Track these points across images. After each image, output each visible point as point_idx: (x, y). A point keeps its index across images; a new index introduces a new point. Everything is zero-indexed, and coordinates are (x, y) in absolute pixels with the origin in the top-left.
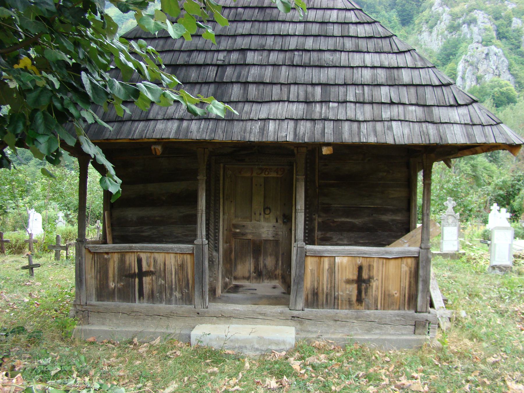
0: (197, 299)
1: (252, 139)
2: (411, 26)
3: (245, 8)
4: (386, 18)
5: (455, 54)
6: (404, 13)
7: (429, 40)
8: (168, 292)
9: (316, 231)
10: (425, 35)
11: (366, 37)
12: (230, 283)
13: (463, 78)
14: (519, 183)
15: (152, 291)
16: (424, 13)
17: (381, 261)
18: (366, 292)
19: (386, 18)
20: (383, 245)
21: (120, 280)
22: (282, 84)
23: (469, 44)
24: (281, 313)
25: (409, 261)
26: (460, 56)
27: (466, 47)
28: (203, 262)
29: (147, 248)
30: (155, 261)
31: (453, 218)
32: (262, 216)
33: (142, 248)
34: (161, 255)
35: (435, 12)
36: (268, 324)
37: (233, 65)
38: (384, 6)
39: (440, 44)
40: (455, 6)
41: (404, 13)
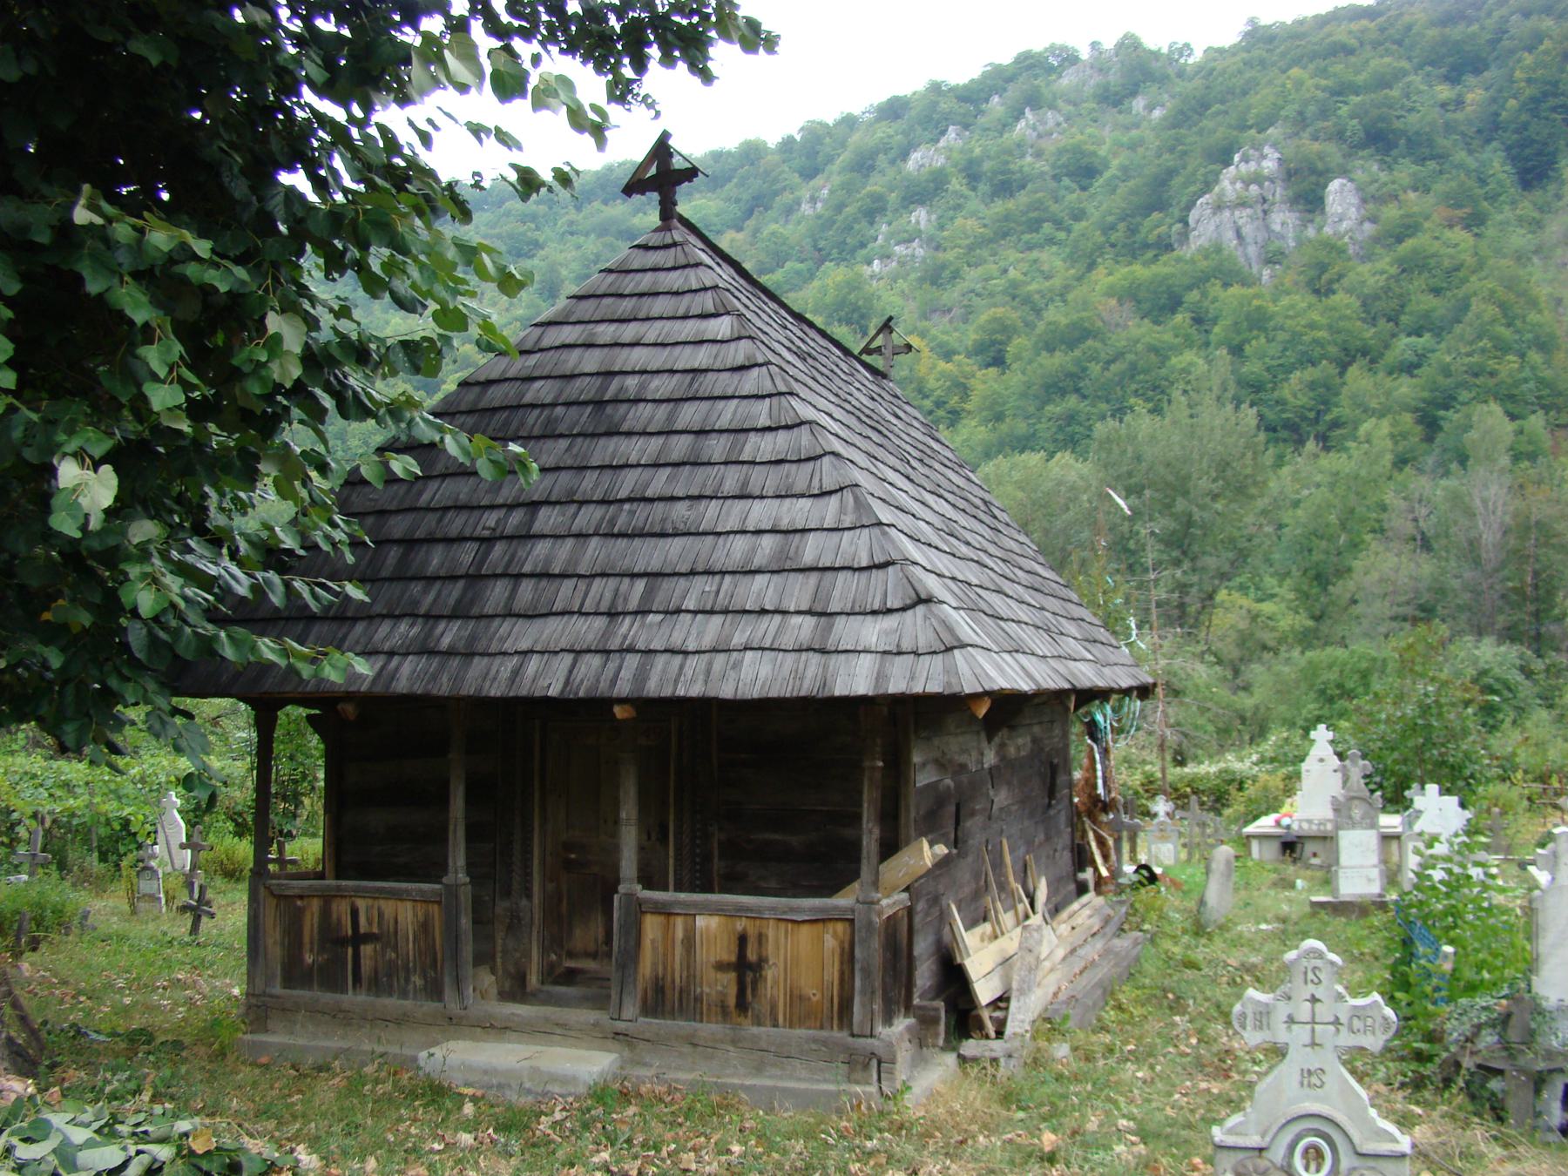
0: (449, 993)
1: (492, 693)
2: (1552, 188)
3: (568, 404)
4: (1468, 172)
6: (1528, 151)
9: (716, 860)
11: (770, 462)
17: (782, 925)
18: (754, 990)
19: (1468, 172)
22: (580, 576)
24: (596, 1025)
25: (840, 927)
29: (365, 889)
30: (381, 915)
31: (1364, 806)
33: (356, 889)
34: (391, 902)
36: (572, 1046)
38: (1463, 134)
41: (1528, 151)
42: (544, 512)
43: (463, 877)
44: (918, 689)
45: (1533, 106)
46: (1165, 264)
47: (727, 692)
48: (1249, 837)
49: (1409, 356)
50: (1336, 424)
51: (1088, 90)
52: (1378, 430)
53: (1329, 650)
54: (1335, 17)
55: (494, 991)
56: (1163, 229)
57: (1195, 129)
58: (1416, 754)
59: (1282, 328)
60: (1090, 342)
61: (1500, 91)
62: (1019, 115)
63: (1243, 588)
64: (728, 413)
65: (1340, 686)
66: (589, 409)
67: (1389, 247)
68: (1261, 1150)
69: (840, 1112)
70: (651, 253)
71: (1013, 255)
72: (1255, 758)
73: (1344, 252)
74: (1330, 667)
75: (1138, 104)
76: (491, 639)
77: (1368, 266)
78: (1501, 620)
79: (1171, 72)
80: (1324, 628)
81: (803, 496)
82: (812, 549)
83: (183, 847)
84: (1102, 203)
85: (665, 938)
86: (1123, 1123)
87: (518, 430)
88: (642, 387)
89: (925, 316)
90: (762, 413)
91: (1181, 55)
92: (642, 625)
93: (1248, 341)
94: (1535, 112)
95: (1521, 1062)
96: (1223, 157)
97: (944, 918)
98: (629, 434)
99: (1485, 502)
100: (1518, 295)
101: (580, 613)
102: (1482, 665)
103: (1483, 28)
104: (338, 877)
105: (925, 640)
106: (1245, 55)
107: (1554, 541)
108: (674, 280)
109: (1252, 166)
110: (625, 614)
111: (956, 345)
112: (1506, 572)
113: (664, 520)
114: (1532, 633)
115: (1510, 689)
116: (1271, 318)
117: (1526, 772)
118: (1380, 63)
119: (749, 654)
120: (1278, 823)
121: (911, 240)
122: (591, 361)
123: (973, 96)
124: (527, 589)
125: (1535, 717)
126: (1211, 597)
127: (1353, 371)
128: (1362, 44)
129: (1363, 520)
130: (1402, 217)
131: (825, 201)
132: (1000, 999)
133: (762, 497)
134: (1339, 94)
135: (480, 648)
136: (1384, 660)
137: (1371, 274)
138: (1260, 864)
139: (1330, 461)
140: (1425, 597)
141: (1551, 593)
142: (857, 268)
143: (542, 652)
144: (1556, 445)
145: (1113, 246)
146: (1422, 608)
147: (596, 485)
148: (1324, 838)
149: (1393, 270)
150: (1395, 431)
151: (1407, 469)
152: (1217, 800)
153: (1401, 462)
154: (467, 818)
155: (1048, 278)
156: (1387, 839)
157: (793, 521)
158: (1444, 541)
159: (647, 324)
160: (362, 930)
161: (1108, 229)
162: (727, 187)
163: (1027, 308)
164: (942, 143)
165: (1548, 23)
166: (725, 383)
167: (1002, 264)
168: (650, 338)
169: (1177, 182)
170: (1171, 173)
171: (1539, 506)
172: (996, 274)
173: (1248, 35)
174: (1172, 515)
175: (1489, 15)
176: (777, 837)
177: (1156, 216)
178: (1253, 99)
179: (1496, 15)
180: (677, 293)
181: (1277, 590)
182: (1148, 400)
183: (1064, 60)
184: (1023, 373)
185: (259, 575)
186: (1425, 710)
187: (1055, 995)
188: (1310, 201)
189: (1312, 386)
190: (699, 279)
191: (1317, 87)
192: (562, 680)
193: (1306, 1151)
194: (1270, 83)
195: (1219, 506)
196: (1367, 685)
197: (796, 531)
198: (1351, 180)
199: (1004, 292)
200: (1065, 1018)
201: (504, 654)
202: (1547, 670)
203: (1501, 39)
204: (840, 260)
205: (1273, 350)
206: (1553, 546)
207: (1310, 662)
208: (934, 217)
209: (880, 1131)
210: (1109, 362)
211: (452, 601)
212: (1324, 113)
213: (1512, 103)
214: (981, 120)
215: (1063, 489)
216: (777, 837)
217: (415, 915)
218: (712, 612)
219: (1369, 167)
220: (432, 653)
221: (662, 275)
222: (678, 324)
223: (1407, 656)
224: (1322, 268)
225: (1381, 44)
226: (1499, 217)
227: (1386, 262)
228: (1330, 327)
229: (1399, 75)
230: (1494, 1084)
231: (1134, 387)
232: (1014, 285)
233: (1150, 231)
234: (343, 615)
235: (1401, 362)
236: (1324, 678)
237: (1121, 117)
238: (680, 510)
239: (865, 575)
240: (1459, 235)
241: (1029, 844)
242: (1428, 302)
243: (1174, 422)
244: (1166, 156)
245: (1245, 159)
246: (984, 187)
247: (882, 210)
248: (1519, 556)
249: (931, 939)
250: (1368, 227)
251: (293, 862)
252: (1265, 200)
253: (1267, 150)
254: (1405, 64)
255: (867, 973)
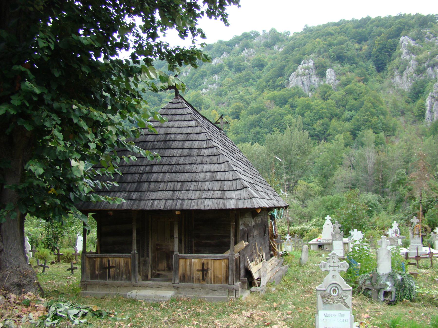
0: (133, 279)
2: (385, 72)
4: (363, 67)
5: (423, 92)
6: (379, 62)
7: (401, 82)
8: (121, 275)
10: (397, 78)
12: (156, 272)
13: (431, 111)
14: (432, 203)
15: (114, 275)
16: (394, 61)
17: (212, 261)
18: (206, 275)
20: (222, 253)
21: (100, 270)
22: (165, 182)
23: (434, 83)
24: (169, 285)
25: (226, 260)
26: (427, 93)
27: (431, 86)
28: (135, 262)
29: (112, 256)
30: (115, 261)
32: (170, 240)
33: (109, 256)
34: (118, 258)
35: (404, 60)
37: (146, 173)
38: (362, 57)
39: (410, 85)
40: (420, 53)
41: (379, 62)
42: (155, 167)
43: (136, 252)
44: (245, 207)
45: (380, 50)
46: (283, 91)
47: (202, 208)
48: (310, 244)
49: (349, 117)
50: (329, 135)
51: (262, 43)
52: (340, 137)
53: (328, 196)
54: (328, 25)
55: (141, 279)
56: (283, 81)
57: (291, 54)
58: (352, 222)
59: (314, 109)
60: (262, 112)
61: (371, 46)
62: (243, 50)
63: (304, 180)
64: (196, 144)
65: (331, 206)
66: (163, 143)
67: (343, 87)
68: (325, 290)
69: (227, 301)
70: (174, 104)
71: (241, 88)
72: (310, 224)
73: (331, 88)
74: (329, 201)
75: (276, 47)
76: (145, 197)
77: (337, 92)
78: (373, 188)
79: (284, 39)
80: (327, 190)
81: (216, 164)
82: (219, 176)
83: (30, 251)
84: (266, 74)
85: (185, 264)
86: (289, 302)
87: (146, 147)
88: (175, 137)
89: (217, 105)
90: (204, 144)
91: (287, 34)
92: (181, 193)
93: (305, 112)
94: (380, 52)
95: (375, 287)
96: (299, 62)
97: (245, 260)
98: (173, 149)
99: (369, 156)
100: (377, 101)
101: (166, 190)
102: (368, 200)
103: (366, 30)
104: (101, 253)
105: (246, 196)
106: (304, 35)
107: (386, 167)
108: (180, 111)
109: (306, 65)
110: (177, 191)
111: (226, 113)
112: (374, 175)
113: (184, 169)
114: (381, 191)
115: (376, 206)
116: (312, 106)
117: (379, 227)
118: (341, 38)
119: (206, 199)
120: (317, 240)
121: (213, 84)
122: (162, 131)
123: (230, 45)
124: (152, 185)
125: (382, 213)
126: (296, 182)
127: (333, 120)
128: (335, 33)
129: (336, 161)
130: (347, 79)
131: (189, 73)
132: (258, 278)
133: (206, 164)
134: (330, 46)
135: (143, 198)
136: (343, 199)
137: (338, 94)
138: (313, 251)
139: (327, 145)
140: (354, 182)
141: (386, 181)
142: (198, 91)
143: (158, 199)
144: (387, 141)
145: (269, 86)
146: (353, 185)
147: (167, 160)
148: (329, 244)
149: (344, 93)
150: (345, 137)
151: (348, 147)
152: (301, 236)
153: (347, 145)
154: (132, 239)
155: (251, 95)
156: (345, 244)
157: (214, 169)
158: (358, 167)
159: (175, 122)
160: (111, 265)
161: (267, 81)
162: (162, 68)
163: (245, 103)
164: (222, 57)
165: (383, 29)
166: (195, 137)
167: (238, 91)
168: (176, 125)
169: (286, 69)
170: (285, 66)
171: (383, 157)
172: (237, 93)
173: (305, 29)
174: (286, 160)
175: (368, 26)
176: (208, 241)
177: (280, 78)
178: (306, 46)
179: (370, 26)
180: (181, 115)
181: (314, 180)
182: (278, 128)
183: (255, 35)
184: (244, 121)
185: (95, 182)
186: (354, 211)
187: (270, 278)
188: (322, 75)
189: (323, 124)
190: (186, 111)
191: (324, 44)
192: (163, 206)
193: (333, 290)
194: (311, 42)
195: (298, 157)
196: (338, 206)
197: (215, 172)
198: (333, 69)
199: (239, 98)
200: (274, 282)
201: (149, 200)
202: (385, 201)
203: (371, 33)
204: (193, 89)
205: (312, 115)
206: (387, 168)
207: (323, 200)
208: (219, 77)
209: (237, 305)
210: (268, 118)
211: (134, 188)
212: (325, 51)
213: (374, 49)
214: (233, 51)
215: (257, 153)
216: (208, 241)
217: (124, 261)
218: (197, 190)
219: (337, 66)
220: (131, 200)
221: (177, 110)
222: (182, 122)
223: (349, 198)
224: (325, 93)
225: (340, 33)
226: (372, 80)
227: (342, 91)
228: (327, 109)
229: (345, 41)
230: (369, 292)
231: (274, 125)
232: (242, 96)
233: (279, 82)
234: (113, 191)
235: (346, 118)
236: (327, 204)
237: (271, 51)
238: (187, 167)
239: (231, 182)
240: (361, 84)
241: (261, 244)
242: (354, 102)
243: (287, 135)
244: (283, 62)
245: (305, 63)
246: (233, 69)
247: (205, 75)
248: (378, 171)
249: (243, 264)
250: (337, 82)
251: (62, 255)
252: (310, 74)
253: (310, 60)
254: (347, 38)
255: (232, 270)
